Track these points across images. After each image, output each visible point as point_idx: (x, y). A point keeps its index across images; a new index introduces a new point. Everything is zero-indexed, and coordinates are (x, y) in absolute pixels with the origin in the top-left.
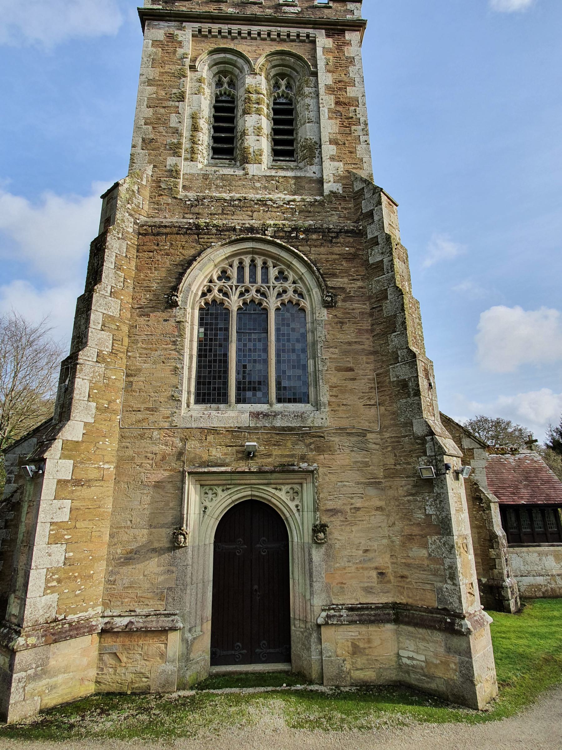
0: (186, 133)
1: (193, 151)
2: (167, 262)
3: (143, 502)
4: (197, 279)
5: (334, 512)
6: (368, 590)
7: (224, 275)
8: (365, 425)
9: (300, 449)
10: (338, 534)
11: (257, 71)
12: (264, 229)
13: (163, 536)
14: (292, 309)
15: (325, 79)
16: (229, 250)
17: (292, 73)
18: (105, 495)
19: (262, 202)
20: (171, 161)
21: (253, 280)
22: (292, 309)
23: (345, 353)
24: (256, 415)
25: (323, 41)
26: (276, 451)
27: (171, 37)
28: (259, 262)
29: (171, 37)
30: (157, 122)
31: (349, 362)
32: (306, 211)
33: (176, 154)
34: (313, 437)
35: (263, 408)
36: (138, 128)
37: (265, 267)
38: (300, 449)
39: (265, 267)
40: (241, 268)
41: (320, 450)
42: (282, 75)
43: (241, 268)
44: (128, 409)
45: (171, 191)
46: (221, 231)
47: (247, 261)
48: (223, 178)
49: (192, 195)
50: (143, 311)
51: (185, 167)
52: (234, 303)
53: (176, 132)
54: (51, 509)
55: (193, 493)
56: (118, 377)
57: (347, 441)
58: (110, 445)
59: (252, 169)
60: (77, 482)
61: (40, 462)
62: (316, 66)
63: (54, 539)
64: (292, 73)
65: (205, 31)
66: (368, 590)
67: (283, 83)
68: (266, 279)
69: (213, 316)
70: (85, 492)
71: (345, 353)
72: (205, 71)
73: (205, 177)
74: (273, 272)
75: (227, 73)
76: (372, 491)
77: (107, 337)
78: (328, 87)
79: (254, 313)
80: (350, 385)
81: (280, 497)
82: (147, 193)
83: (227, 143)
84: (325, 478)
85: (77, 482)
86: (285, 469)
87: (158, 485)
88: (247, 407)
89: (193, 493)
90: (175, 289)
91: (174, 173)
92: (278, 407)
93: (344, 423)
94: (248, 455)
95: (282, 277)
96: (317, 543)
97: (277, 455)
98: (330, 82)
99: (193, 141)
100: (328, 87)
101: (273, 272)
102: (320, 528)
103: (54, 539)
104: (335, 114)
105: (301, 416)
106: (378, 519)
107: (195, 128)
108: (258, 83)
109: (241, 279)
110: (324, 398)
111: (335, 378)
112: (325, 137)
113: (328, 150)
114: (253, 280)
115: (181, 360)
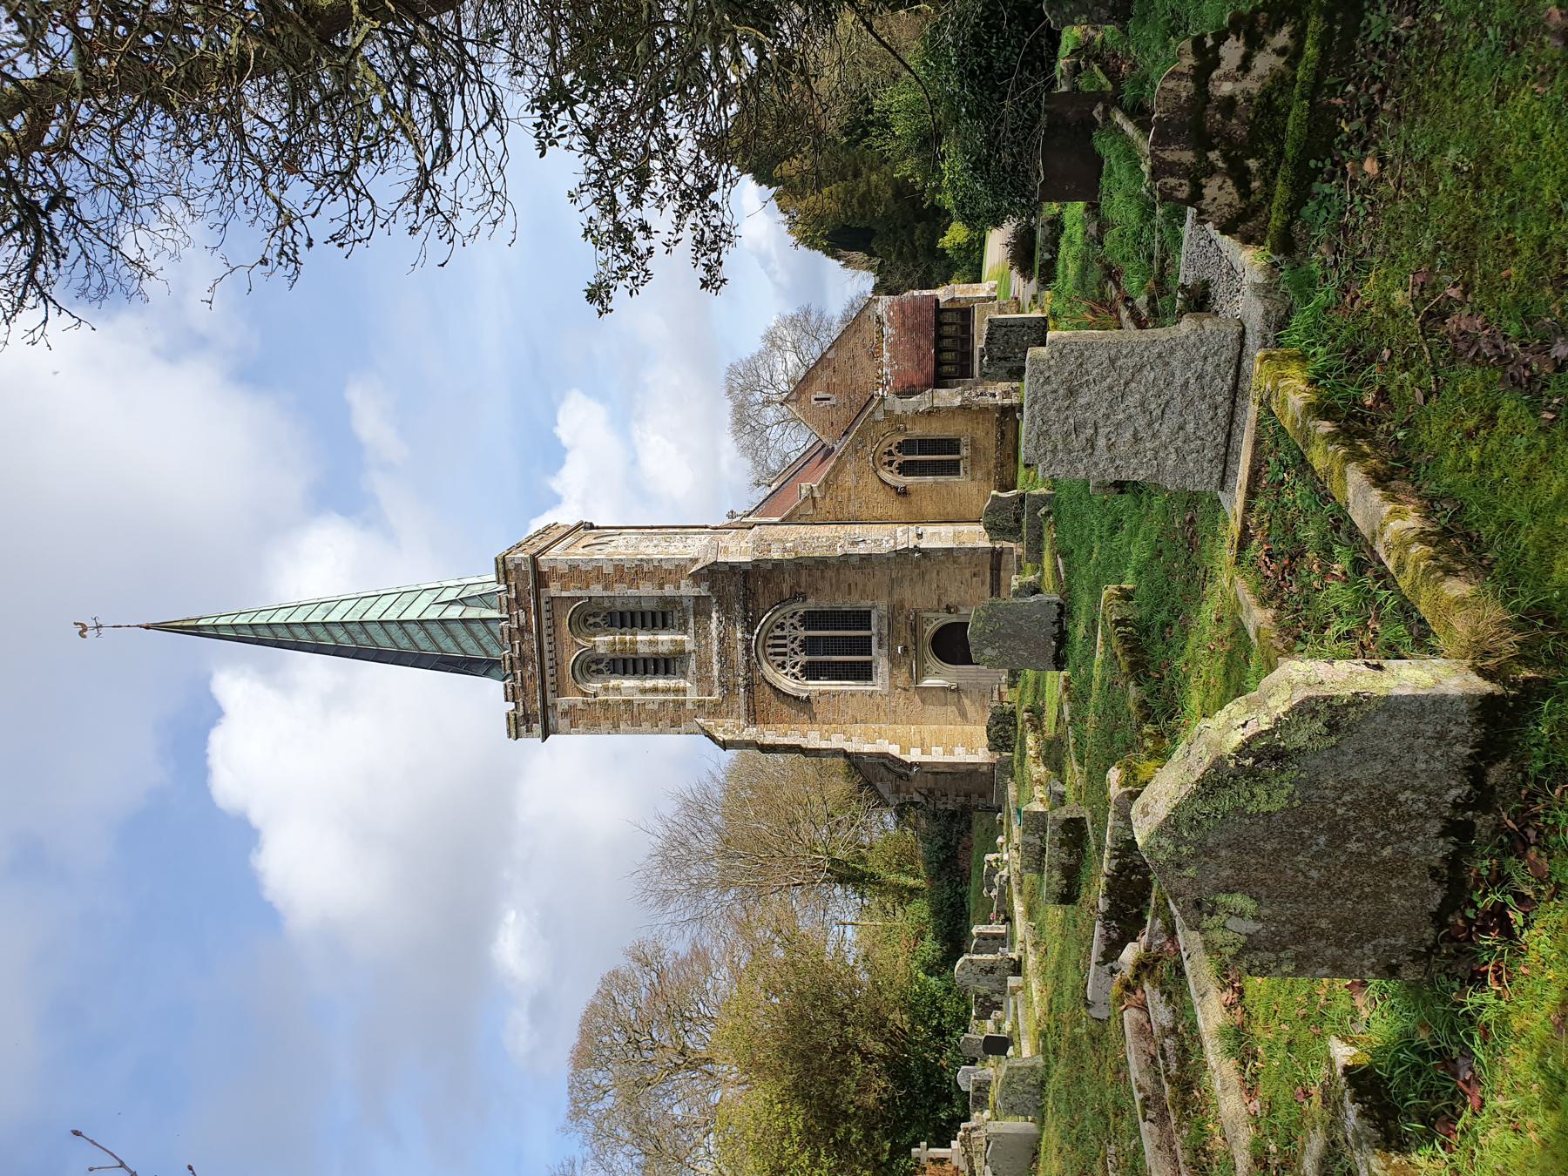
0: (662, 697)
1: (677, 691)
2: (775, 703)
3: (931, 710)
4: (788, 684)
5: (939, 600)
6: (983, 583)
7: (782, 665)
8: (887, 578)
9: (901, 618)
10: (952, 599)
11: (590, 645)
12: (745, 640)
13: (952, 697)
14: (810, 620)
15: (597, 590)
16: (765, 664)
17: (591, 616)
18: (928, 729)
19: (721, 641)
20: (689, 706)
21: (785, 646)
22: (810, 620)
23: (838, 589)
24: (880, 646)
25: (554, 589)
26: (903, 634)
27: (565, 714)
28: (771, 642)
29: (565, 714)
30: (1010, 531)
31: (844, 587)
32: (726, 610)
33: (684, 703)
34: (896, 610)
35: (874, 640)
36: (661, 732)
37: (775, 638)
38: (901, 618)
39: (775, 638)
40: (776, 654)
41: (902, 607)
42: (586, 620)
43: (776, 654)
44: (877, 721)
45: (716, 704)
46: (749, 669)
47: (771, 650)
48: (699, 668)
49: (717, 691)
50: (813, 718)
51: (692, 696)
52: (803, 658)
53: (663, 704)
54: (937, 756)
55: (928, 682)
56: (859, 728)
57: (897, 590)
58: (900, 729)
59: (689, 647)
60: (922, 745)
61: (912, 764)
62: (580, 598)
63: (952, 753)
64: (591, 616)
65: (554, 687)
66: (983, 583)
67: (591, 620)
68: (784, 638)
69: (812, 672)
70: (927, 741)
71: (838, 589)
72: (594, 686)
73: (699, 681)
74: (778, 632)
75: (592, 666)
76: (927, 577)
77: (834, 737)
78: (606, 588)
79: (809, 645)
80: (860, 586)
81: (930, 629)
82: (720, 721)
83: (663, 665)
84: (919, 603)
85: (922, 745)
86: (914, 630)
87: (923, 701)
88: (874, 649)
89: (928, 682)
90: (797, 698)
91: (700, 705)
92: (874, 630)
93: (886, 592)
94: (905, 649)
95: (781, 626)
96: (957, 610)
97: (905, 633)
98: (600, 587)
99: (667, 691)
100: (606, 588)
101: (778, 632)
102: (948, 609)
103: (952, 753)
104: (633, 583)
105: (880, 618)
106: (943, 575)
107: (655, 690)
108: (603, 642)
109: (784, 654)
110: (870, 603)
111: (856, 596)
112: (658, 593)
113: (669, 590)
114: (785, 646)
115: (846, 692)
